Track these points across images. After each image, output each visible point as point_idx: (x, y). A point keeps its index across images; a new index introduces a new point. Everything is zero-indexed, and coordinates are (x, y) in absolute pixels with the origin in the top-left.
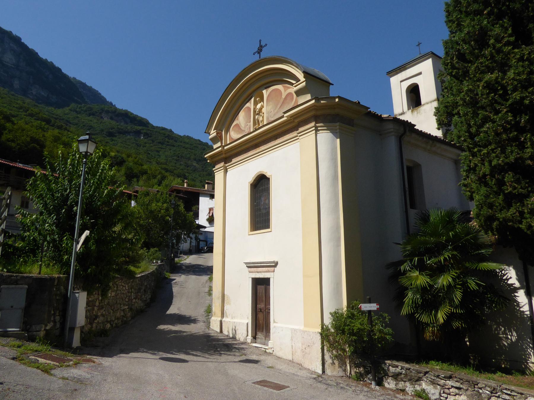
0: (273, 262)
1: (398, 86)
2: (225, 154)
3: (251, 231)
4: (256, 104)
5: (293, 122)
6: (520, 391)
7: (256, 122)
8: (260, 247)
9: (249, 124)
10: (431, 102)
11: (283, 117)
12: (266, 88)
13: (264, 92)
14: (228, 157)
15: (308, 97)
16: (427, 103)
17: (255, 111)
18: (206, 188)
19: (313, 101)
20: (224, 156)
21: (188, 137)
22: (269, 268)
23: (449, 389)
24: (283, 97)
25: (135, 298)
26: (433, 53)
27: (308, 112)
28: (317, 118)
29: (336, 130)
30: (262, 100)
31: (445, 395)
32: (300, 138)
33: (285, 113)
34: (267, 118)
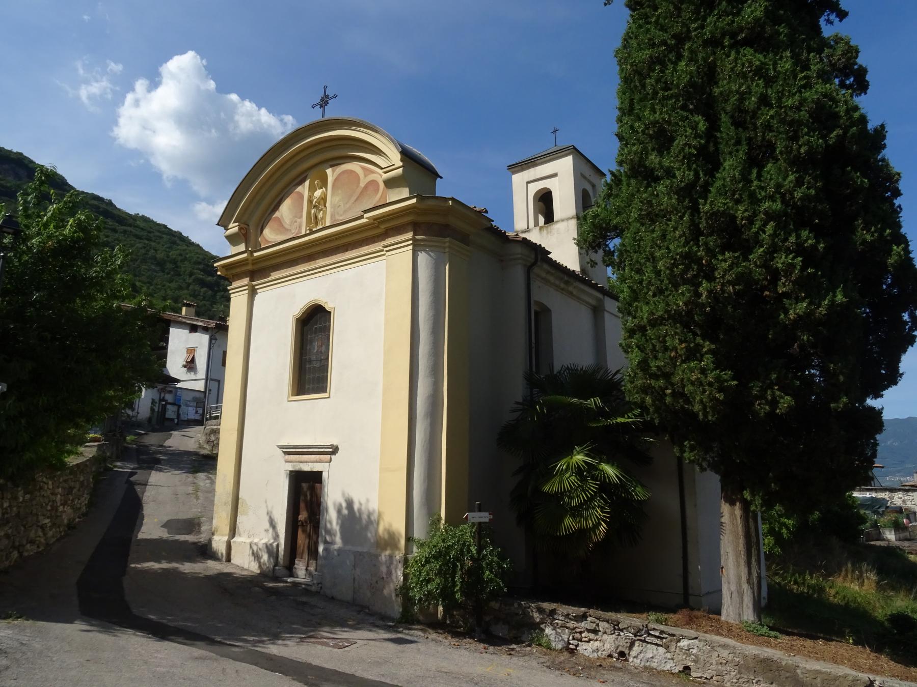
0: (332, 446)
1: (523, 187)
2: (253, 264)
3: (293, 395)
4: (312, 189)
5: (378, 227)
6: (671, 632)
7: (313, 220)
8: (309, 421)
9: (299, 220)
10: (568, 219)
11: (361, 217)
12: (331, 166)
13: (329, 171)
14: (258, 270)
15: (405, 192)
16: (563, 220)
17: (310, 201)
18: (184, 313)
19: (414, 201)
20: (250, 267)
21: (145, 219)
22: (322, 456)
23: (581, 633)
24: (362, 185)
25: (64, 504)
26: (574, 148)
27: (407, 215)
28: (416, 227)
29: (444, 248)
30: (324, 183)
31: (575, 642)
32: (388, 254)
33: (366, 211)
34: (332, 216)
